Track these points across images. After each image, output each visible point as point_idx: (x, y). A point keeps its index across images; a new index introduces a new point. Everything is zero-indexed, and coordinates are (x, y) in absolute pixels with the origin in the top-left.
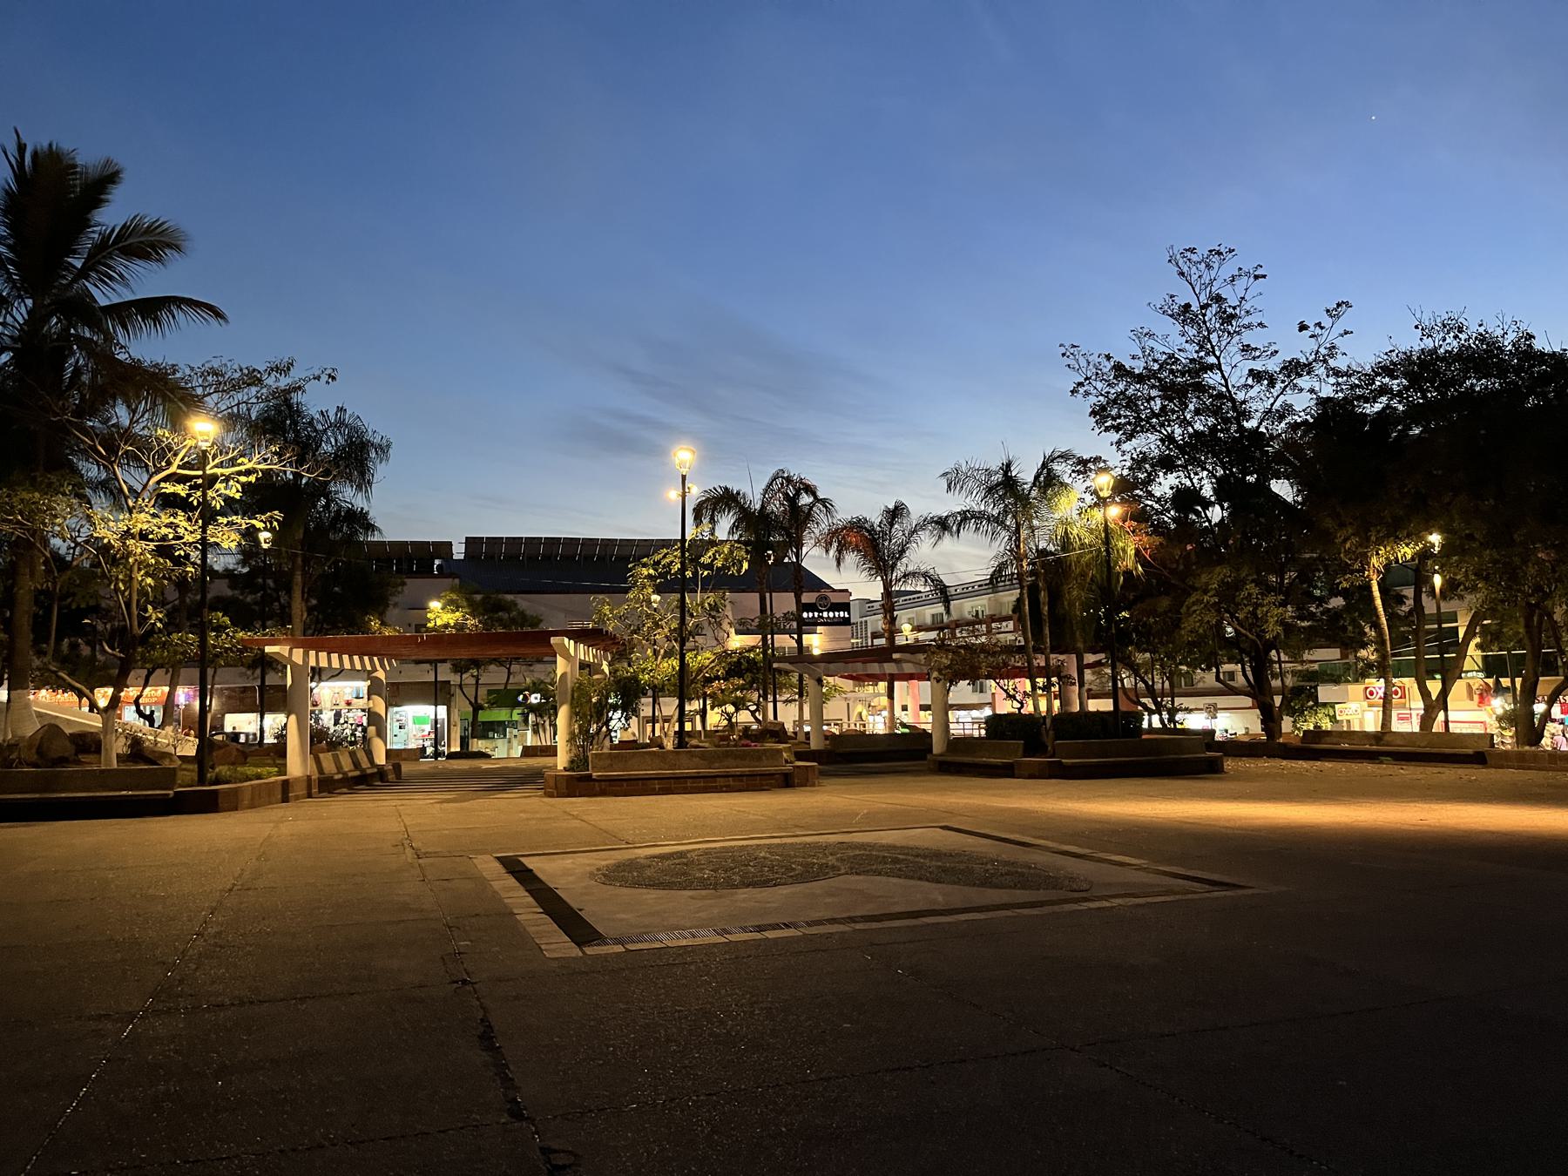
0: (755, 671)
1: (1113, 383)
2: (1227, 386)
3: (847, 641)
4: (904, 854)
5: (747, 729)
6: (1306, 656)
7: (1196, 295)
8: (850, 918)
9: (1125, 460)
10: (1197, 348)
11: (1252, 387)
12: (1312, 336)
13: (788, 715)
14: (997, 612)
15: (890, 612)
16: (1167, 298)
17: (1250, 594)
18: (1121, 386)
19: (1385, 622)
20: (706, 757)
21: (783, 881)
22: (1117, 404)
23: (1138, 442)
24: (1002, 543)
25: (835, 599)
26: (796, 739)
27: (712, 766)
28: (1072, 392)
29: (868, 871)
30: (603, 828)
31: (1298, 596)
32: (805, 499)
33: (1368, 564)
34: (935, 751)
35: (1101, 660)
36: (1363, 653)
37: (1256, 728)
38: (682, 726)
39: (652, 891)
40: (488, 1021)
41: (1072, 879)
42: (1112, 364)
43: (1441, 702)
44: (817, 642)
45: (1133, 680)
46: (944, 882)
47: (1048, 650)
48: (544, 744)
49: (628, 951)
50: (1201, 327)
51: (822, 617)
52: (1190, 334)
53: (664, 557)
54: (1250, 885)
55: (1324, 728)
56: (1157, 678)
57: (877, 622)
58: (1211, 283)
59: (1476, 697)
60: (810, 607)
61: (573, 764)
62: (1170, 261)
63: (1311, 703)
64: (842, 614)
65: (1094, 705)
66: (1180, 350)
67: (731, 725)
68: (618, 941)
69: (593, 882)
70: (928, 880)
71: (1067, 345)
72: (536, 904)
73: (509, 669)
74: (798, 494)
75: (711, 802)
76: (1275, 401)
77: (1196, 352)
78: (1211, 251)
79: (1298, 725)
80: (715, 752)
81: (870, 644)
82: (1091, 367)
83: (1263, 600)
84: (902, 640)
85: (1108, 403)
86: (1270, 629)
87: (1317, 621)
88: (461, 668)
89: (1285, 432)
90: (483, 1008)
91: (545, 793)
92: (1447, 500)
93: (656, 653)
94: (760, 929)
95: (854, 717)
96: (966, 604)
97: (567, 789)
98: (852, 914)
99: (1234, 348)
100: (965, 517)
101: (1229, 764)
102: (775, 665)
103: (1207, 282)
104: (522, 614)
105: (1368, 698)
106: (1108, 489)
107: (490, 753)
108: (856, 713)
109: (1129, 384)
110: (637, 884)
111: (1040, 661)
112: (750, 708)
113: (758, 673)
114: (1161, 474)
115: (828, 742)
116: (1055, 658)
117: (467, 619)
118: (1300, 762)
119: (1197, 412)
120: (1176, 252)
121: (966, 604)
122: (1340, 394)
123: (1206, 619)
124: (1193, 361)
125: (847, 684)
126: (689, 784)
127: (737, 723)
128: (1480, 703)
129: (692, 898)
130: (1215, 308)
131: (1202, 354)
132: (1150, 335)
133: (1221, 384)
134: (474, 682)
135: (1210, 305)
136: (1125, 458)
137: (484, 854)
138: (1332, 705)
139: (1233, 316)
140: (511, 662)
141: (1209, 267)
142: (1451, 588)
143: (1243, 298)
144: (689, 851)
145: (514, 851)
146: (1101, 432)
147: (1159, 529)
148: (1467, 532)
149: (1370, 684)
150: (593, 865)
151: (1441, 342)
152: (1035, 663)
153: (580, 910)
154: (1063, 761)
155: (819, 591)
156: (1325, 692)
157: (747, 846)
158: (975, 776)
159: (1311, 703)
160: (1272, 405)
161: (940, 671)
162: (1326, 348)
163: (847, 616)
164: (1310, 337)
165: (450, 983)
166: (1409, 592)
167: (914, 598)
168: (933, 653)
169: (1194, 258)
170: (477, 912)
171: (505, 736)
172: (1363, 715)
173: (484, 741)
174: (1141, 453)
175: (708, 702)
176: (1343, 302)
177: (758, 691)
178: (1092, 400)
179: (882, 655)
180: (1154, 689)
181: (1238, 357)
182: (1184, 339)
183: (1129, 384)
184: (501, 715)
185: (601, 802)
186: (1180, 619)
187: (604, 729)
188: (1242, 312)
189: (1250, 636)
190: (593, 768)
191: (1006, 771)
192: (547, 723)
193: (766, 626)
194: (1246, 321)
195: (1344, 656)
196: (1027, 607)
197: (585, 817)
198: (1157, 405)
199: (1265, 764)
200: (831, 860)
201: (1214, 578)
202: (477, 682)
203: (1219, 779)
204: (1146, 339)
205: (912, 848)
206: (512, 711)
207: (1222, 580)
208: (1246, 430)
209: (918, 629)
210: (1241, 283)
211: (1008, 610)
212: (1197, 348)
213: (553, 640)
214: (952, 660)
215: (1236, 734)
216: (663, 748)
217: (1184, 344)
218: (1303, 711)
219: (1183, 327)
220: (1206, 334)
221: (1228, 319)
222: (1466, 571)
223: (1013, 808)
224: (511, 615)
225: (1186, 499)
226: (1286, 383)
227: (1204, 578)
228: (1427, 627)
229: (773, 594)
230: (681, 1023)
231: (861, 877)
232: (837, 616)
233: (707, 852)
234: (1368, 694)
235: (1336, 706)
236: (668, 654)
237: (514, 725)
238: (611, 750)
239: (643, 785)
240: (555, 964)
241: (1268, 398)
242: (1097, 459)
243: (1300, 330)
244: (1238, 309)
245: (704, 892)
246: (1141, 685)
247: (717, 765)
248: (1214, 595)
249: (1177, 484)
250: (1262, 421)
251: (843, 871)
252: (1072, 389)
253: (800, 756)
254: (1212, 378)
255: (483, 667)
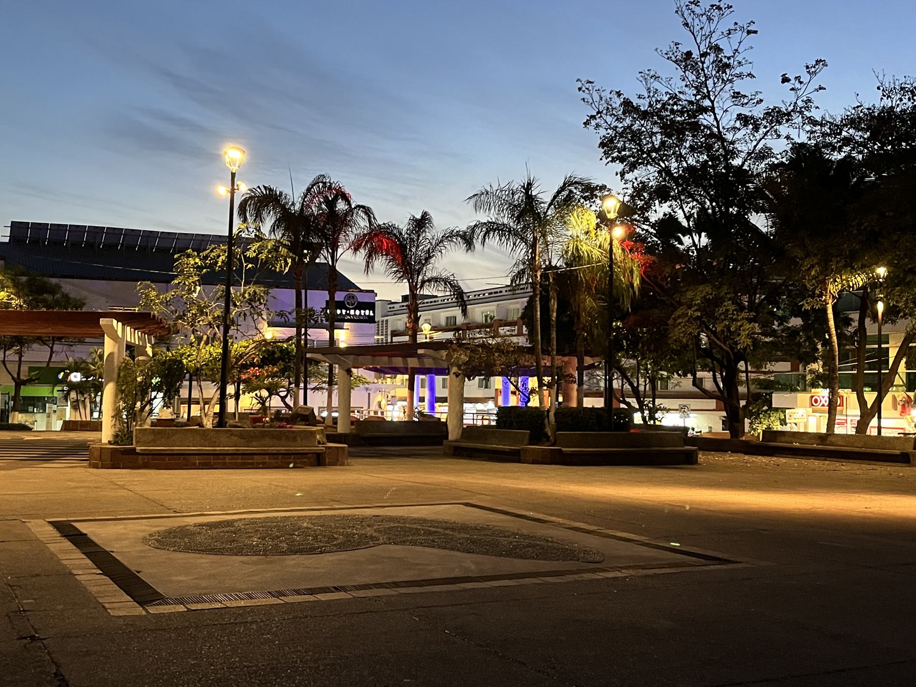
0: (287, 360)
1: (621, 118)
2: (718, 128)
3: (372, 337)
4: (434, 527)
5: (278, 412)
6: (769, 367)
7: (698, 44)
8: (394, 583)
9: (627, 189)
10: (695, 92)
11: (739, 129)
12: (792, 89)
13: (317, 401)
14: (504, 318)
15: (414, 312)
16: (672, 45)
17: (727, 310)
18: (628, 121)
19: (836, 340)
20: (247, 438)
21: (328, 549)
22: (623, 137)
23: (639, 172)
24: (521, 252)
25: (362, 298)
26: (324, 423)
27: (250, 445)
28: (585, 123)
29: (404, 542)
30: (150, 497)
31: (760, 315)
32: (341, 206)
33: (826, 289)
34: (450, 437)
35: (594, 364)
36: (814, 366)
37: (718, 427)
38: (223, 406)
39: (204, 556)
40: (62, 675)
41: (585, 552)
42: (622, 100)
43: (876, 408)
44: (344, 337)
45: (620, 382)
46: (474, 552)
47: (555, 352)
48: (84, 419)
49: (189, 610)
50: (700, 74)
51: (349, 314)
52: (690, 79)
53: (212, 251)
54: (737, 560)
55: (775, 430)
56: (641, 381)
57: (401, 321)
58: (711, 33)
59: (899, 407)
60: (341, 305)
61: (117, 438)
62: (677, 12)
63: (765, 408)
64: (367, 312)
65: (588, 403)
66: (680, 92)
67: (264, 409)
68: (180, 601)
69: (147, 547)
70: (458, 550)
71: (584, 80)
72: (95, 567)
73: (52, 348)
74: (335, 199)
75: (250, 477)
76: (757, 144)
77: (694, 95)
78: (712, 6)
79: (754, 427)
80: (253, 432)
81: (389, 341)
82: (603, 102)
83: (738, 315)
84: (422, 339)
85: (616, 136)
86: (742, 341)
87: (777, 337)
88: (5, 346)
89: (765, 171)
90: (56, 664)
91: (90, 464)
92: (895, 238)
93: (199, 339)
94: (312, 592)
95: (374, 407)
96: (476, 309)
97: (111, 461)
98: (395, 580)
99: (726, 95)
100: (491, 228)
101: (701, 457)
102: (308, 355)
103: (707, 34)
104: (66, 297)
105: (813, 405)
106: (615, 212)
107: (31, 426)
108: (376, 403)
109: (634, 119)
110: (188, 549)
111: (546, 362)
112: (280, 394)
113: (289, 362)
114: (657, 202)
115: (353, 427)
116: (559, 360)
117: (12, 299)
118: (760, 457)
119: (692, 149)
120: (682, 5)
121: (476, 309)
122: (812, 141)
123: (690, 330)
124: (691, 103)
125: (369, 375)
126: (227, 460)
127: (270, 407)
128: (902, 412)
129: (243, 562)
130: (712, 57)
131: (698, 97)
132: (655, 77)
133: (714, 126)
134: (17, 359)
135: (709, 54)
136: (627, 186)
137: (37, 518)
138: (783, 410)
139: (728, 66)
140: (54, 341)
141: (709, 19)
142: (892, 313)
143: (736, 50)
144: (236, 521)
145: (67, 517)
146: (608, 163)
147: (651, 250)
148: (910, 266)
149: (814, 393)
150: (144, 531)
151: (898, 102)
152: (542, 363)
153: (138, 572)
154: (563, 449)
155: (348, 291)
156: (778, 399)
157: (289, 517)
158: (485, 460)
159: (765, 408)
160: (755, 146)
161: (459, 367)
162: (802, 101)
163: (372, 314)
164: (791, 90)
165: (18, 639)
166: (855, 316)
167: (431, 302)
168: (454, 350)
169: (698, 10)
170: (37, 573)
171: (44, 411)
172: (807, 419)
173: (23, 415)
174: (641, 182)
175: (241, 387)
176: (821, 61)
177: (289, 379)
178: (602, 132)
179: (410, 349)
180: (638, 391)
181: (729, 103)
182: (684, 83)
183: (634, 119)
184: (43, 391)
185: (144, 474)
186: (667, 329)
187: (148, 408)
188: (736, 63)
189: (725, 347)
190: (137, 442)
191: (513, 457)
192: (87, 401)
193: (304, 319)
194: (738, 71)
195: (795, 368)
196: (539, 313)
197: (131, 488)
198: (657, 140)
199: (730, 458)
200: (369, 531)
201: (699, 294)
202: (20, 359)
203: (694, 469)
204: (652, 80)
205: (441, 522)
206: (54, 387)
207: (705, 297)
208: (732, 167)
209: (435, 329)
210: (736, 37)
211: (515, 316)
212: (695, 92)
213: (103, 321)
214: (470, 357)
215: (701, 432)
216: (203, 427)
217: (684, 88)
218: (759, 414)
219: (684, 72)
220: (704, 79)
221: (723, 67)
222: (907, 299)
223: (524, 489)
224: (55, 298)
225: (669, 226)
226: (768, 129)
227: (690, 295)
228: (867, 346)
229: (308, 291)
230: (251, 678)
231: (400, 547)
232: (363, 314)
233: (253, 522)
234: (814, 401)
235: (787, 411)
236: (210, 341)
237: (53, 400)
238: (151, 426)
239: (184, 459)
240: (121, 622)
241: (752, 141)
242: (603, 188)
243: (783, 82)
244: (732, 59)
245: (255, 558)
246: (627, 386)
247: (254, 444)
248: (696, 310)
249: (670, 211)
250: (745, 160)
251: (381, 541)
252: (585, 121)
253: (331, 438)
254: (706, 119)
255: (26, 345)
